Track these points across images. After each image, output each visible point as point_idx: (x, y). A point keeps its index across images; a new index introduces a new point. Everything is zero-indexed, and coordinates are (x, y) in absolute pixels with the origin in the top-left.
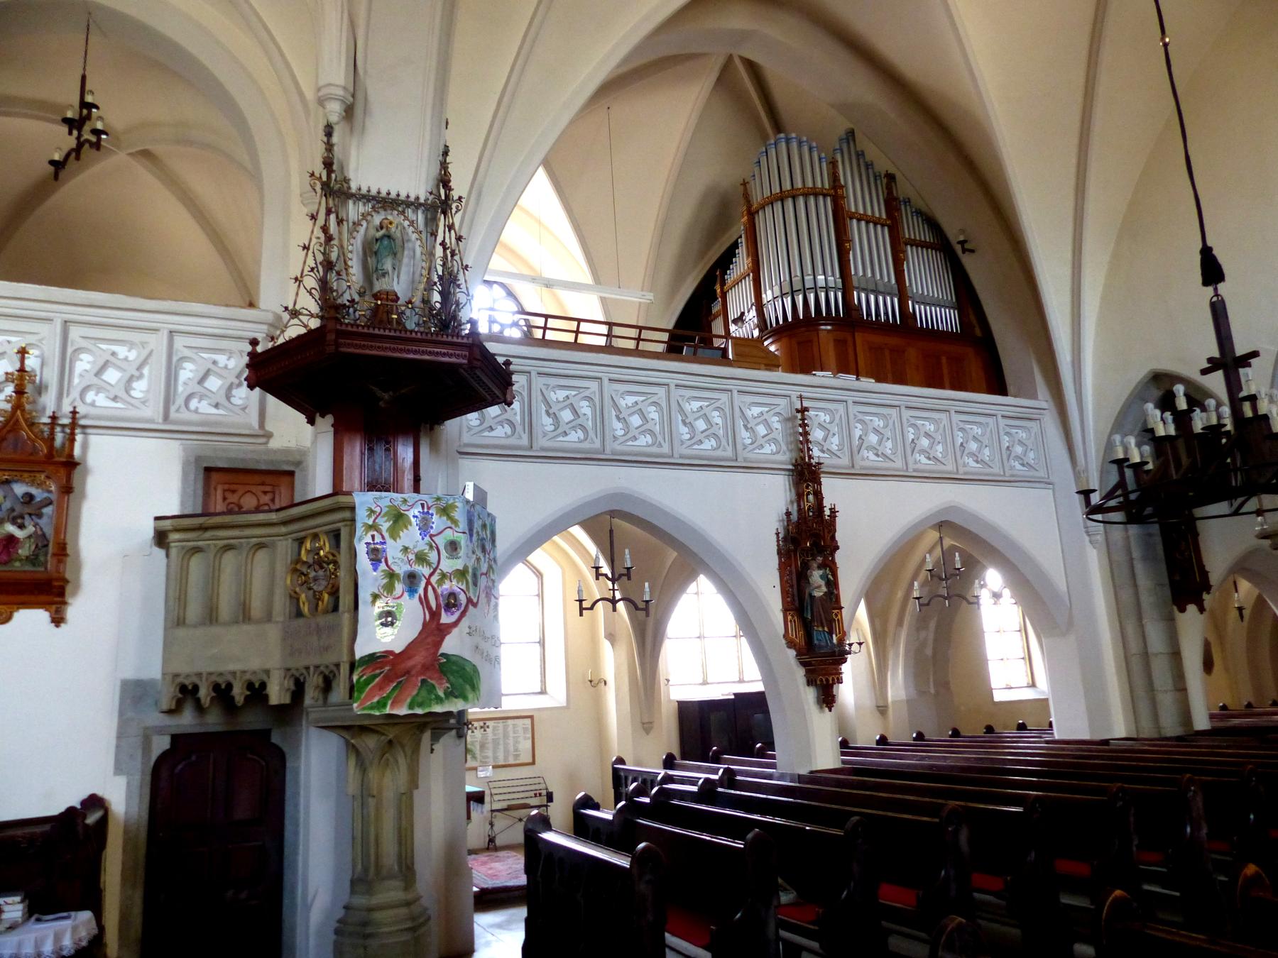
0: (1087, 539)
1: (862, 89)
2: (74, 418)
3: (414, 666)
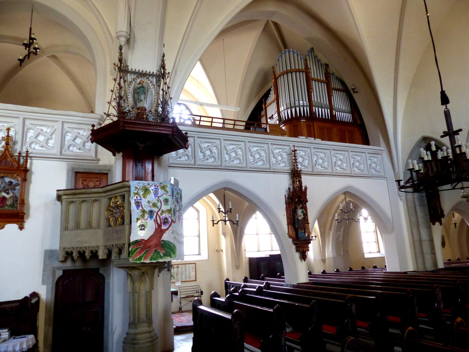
0: (399, 198)
1: (316, 33)
2: (27, 154)
3: (152, 245)
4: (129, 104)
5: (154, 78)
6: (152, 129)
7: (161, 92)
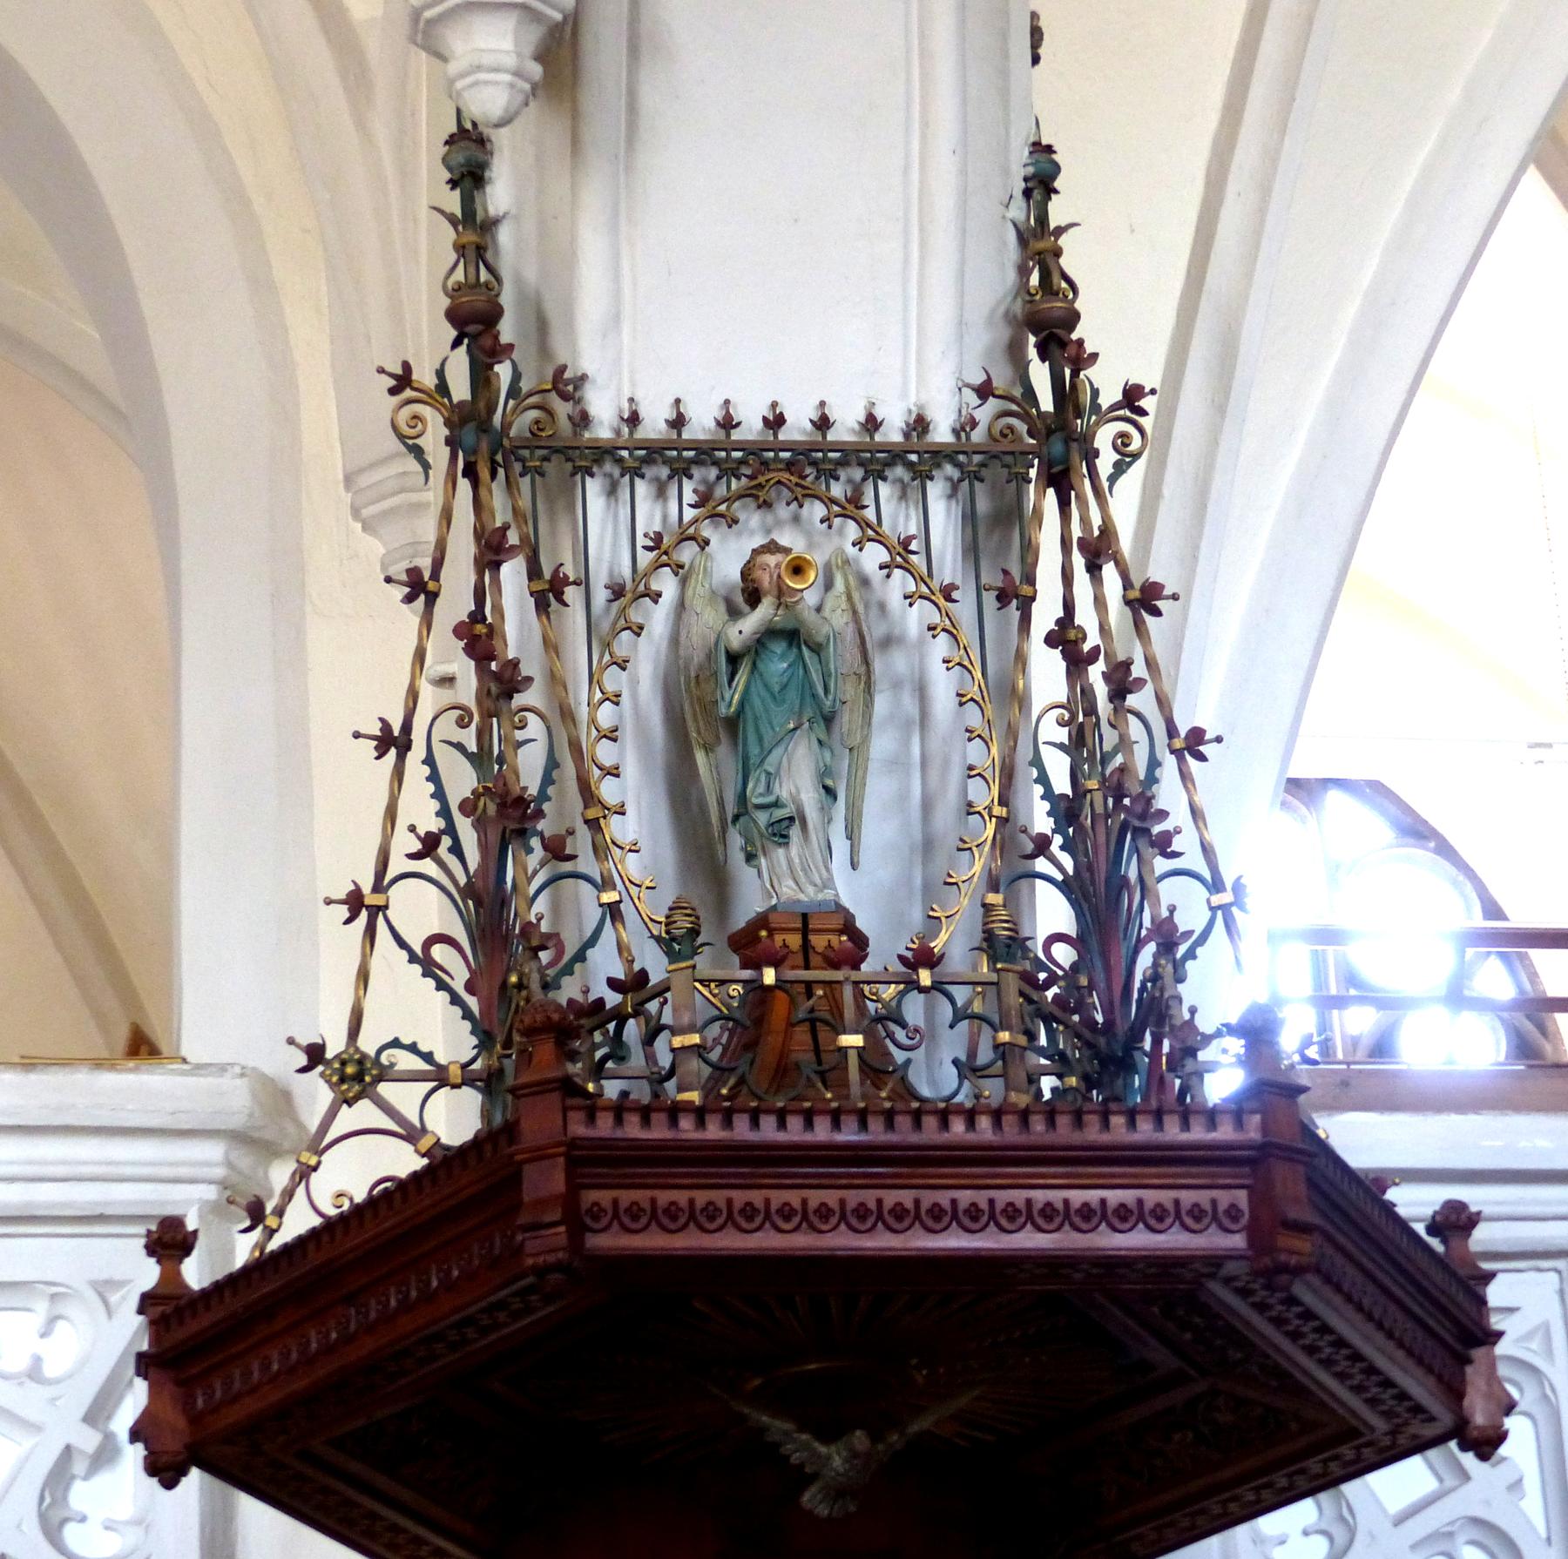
4: (619, 903)
6: (973, 1218)
7: (1047, 676)
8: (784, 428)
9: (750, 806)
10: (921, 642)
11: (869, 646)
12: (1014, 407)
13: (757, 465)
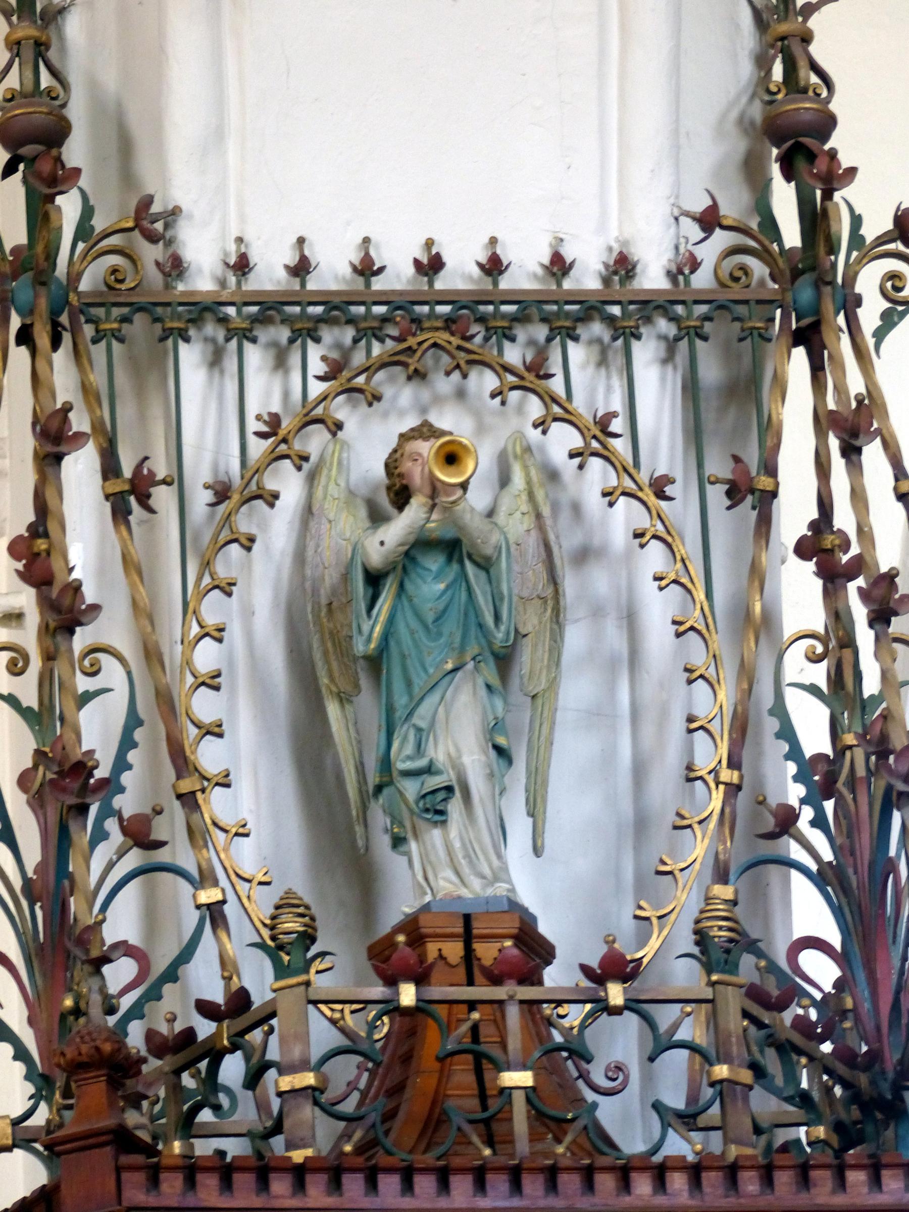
5: (645, 353)
7: (799, 598)
8: (442, 273)
9: (395, 774)
10: (628, 556)
11: (557, 561)
12: (752, 243)
13: (405, 324)
